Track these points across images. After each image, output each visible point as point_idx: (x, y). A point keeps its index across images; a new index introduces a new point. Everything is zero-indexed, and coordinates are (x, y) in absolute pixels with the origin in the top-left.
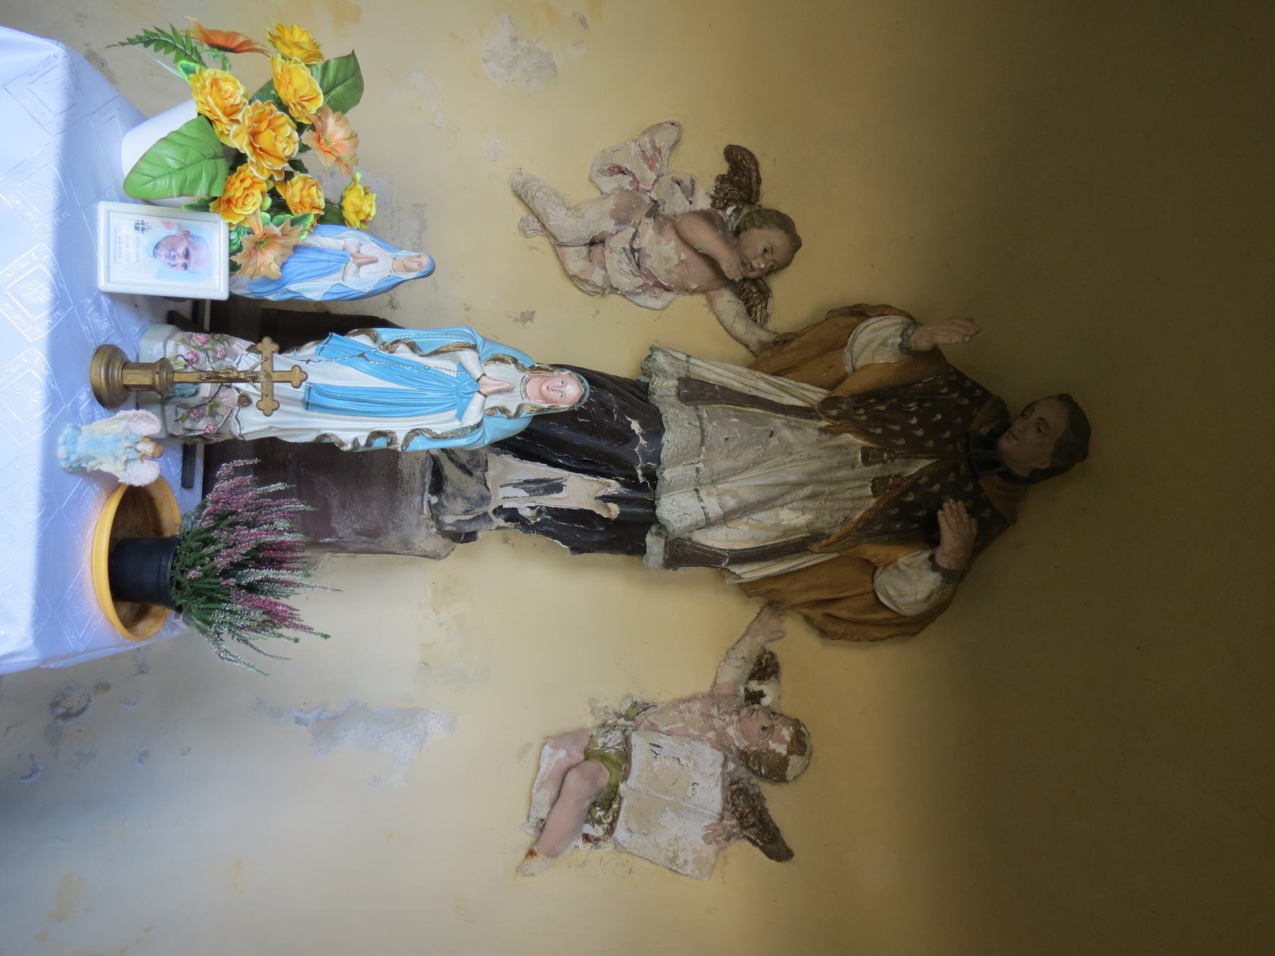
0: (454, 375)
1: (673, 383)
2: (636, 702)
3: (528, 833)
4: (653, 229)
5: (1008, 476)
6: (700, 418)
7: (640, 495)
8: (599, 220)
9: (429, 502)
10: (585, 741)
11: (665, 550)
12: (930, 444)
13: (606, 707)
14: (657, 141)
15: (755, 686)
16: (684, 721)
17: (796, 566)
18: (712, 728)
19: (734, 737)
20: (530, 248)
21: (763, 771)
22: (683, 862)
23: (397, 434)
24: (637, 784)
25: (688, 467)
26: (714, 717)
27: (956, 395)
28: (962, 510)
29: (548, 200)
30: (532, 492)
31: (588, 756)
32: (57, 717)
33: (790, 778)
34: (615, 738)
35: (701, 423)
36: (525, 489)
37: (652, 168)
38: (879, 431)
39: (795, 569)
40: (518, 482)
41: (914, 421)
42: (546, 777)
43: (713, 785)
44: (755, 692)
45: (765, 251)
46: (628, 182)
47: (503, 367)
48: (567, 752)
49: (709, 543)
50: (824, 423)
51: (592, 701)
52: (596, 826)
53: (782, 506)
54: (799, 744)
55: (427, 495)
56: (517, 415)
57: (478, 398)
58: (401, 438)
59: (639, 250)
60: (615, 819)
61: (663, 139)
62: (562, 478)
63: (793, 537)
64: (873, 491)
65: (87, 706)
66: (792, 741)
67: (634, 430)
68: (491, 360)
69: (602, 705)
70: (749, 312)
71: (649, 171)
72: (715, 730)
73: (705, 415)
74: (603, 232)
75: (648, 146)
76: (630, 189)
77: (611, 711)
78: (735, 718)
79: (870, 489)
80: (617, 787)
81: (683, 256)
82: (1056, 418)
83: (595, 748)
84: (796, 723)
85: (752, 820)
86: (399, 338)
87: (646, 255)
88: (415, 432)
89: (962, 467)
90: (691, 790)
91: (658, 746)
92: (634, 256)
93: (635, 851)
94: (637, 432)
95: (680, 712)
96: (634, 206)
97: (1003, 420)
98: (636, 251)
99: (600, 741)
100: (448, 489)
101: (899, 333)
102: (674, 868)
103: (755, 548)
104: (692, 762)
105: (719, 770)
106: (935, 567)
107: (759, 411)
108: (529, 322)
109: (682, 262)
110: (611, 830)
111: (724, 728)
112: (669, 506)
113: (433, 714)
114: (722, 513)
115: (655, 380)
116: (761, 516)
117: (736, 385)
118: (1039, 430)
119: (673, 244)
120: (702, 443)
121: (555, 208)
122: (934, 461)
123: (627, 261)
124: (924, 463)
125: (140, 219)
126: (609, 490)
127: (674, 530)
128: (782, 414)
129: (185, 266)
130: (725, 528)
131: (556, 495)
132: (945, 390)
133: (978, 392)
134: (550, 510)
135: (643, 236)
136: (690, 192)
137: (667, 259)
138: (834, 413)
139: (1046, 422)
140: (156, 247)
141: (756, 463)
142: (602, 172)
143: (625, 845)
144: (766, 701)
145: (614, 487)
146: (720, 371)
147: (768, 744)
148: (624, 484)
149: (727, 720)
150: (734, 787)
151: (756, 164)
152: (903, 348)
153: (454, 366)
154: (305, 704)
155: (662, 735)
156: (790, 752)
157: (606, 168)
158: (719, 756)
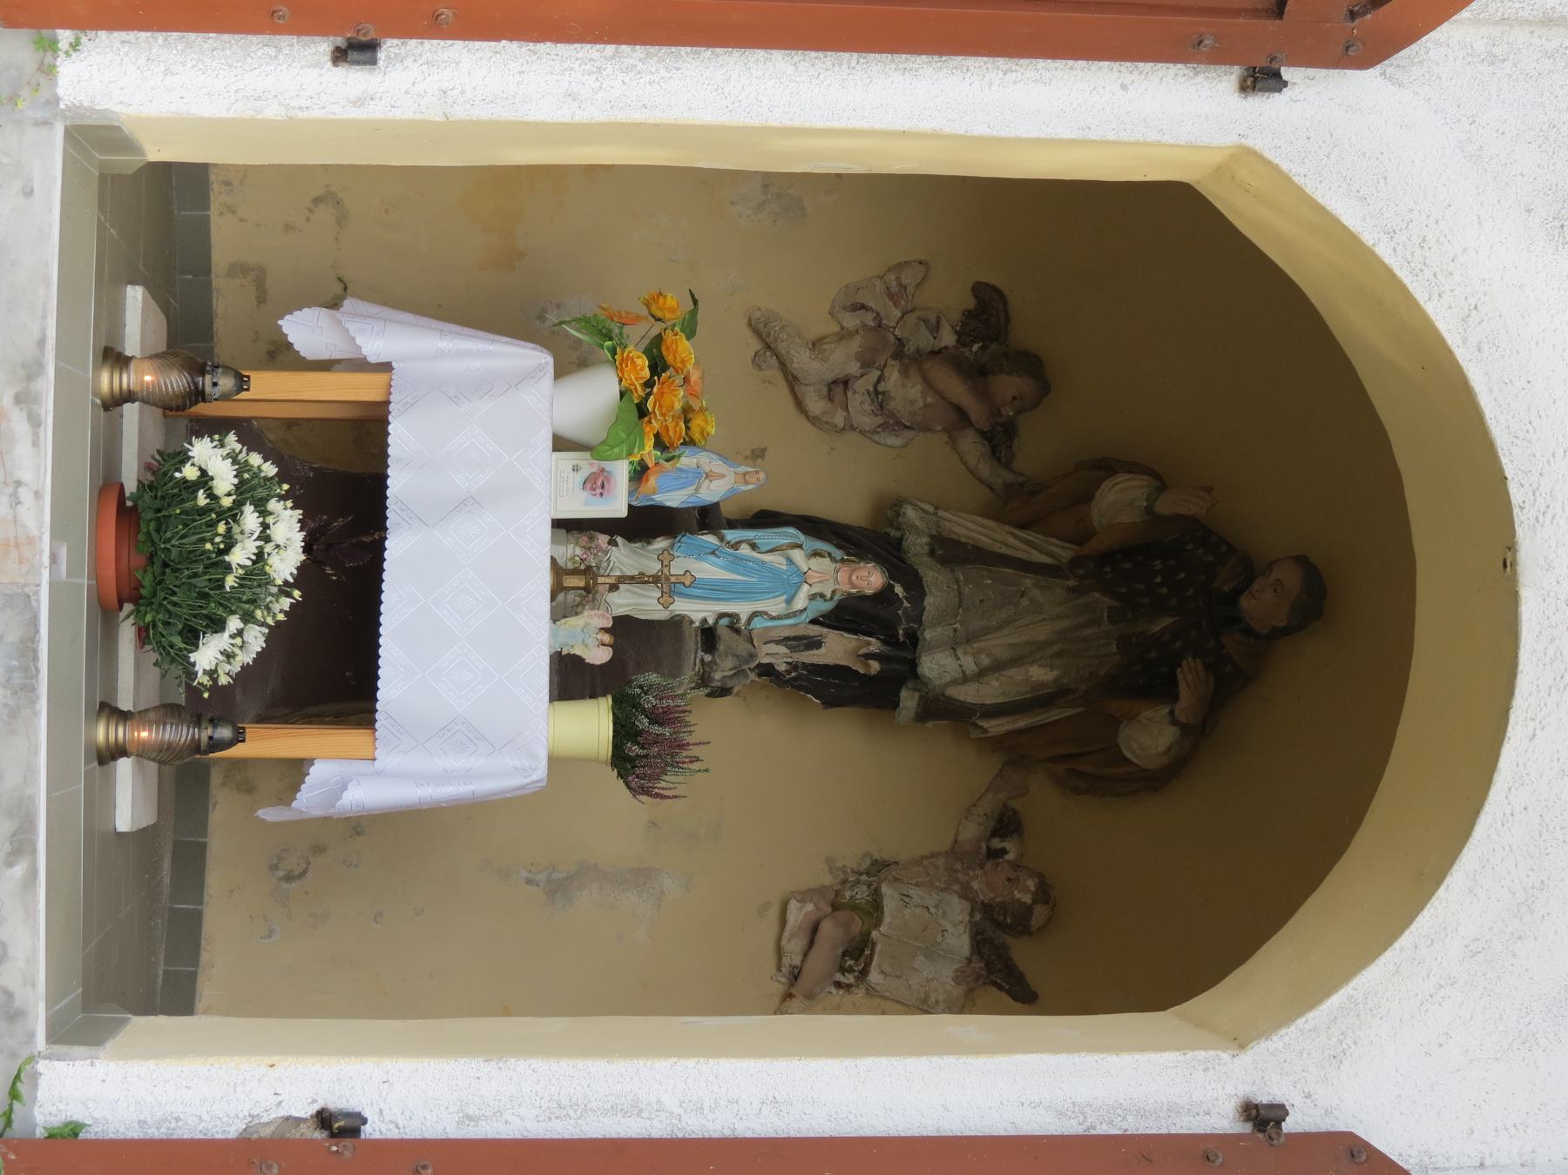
0: (785, 568)
1: (925, 540)
2: (876, 860)
3: (780, 982)
4: (899, 371)
5: (1248, 632)
6: (957, 581)
7: (900, 653)
8: (842, 359)
9: (702, 660)
10: (831, 896)
11: (919, 705)
12: (1174, 602)
13: (845, 866)
14: (903, 277)
15: (997, 843)
16: (929, 875)
17: (1043, 720)
18: (958, 881)
19: (979, 891)
20: (764, 382)
21: (1008, 920)
22: (934, 1002)
23: (741, 616)
24: (890, 931)
25: (946, 628)
26: (959, 872)
27: (1201, 551)
28: (1200, 667)
29: (792, 343)
30: (793, 649)
31: (835, 907)
32: (280, 879)
33: (1033, 929)
34: (862, 894)
35: (959, 586)
36: (786, 646)
37: (896, 304)
38: (1124, 590)
39: (1041, 723)
40: (777, 639)
41: (1158, 580)
42: (795, 929)
43: (962, 931)
44: (998, 850)
45: (1014, 398)
46: (871, 318)
47: (820, 560)
48: (815, 905)
49: (961, 698)
50: (1072, 583)
51: (830, 861)
52: (847, 974)
53: (1031, 664)
54: (1044, 893)
55: (700, 654)
56: (831, 599)
57: (806, 587)
58: (744, 618)
59: (883, 393)
60: (868, 964)
61: (909, 278)
62: (822, 635)
63: (1040, 693)
64: (1118, 648)
65: (307, 868)
66: (1037, 890)
67: (897, 594)
68: (812, 555)
69: (839, 864)
70: (994, 451)
71: (894, 309)
72: (961, 883)
73: (962, 578)
74: (848, 374)
75: (894, 283)
76: (873, 325)
77: (849, 870)
78: (979, 872)
79: (1115, 646)
80: (869, 934)
81: (929, 400)
82: (1290, 576)
83: (843, 901)
84: (1041, 877)
85: (998, 966)
86: (741, 539)
87: (891, 398)
88: (754, 615)
89: (1204, 624)
90: (940, 936)
91: (907, 896)
92: (878, 398)
93: (887, 994)
94: (901, 595)
95: (924, 868)
96: (880, 347)
97: (1249, 572)
98: (880, 393)
99: (848, 894)
100: (721, 647)
101: (1144, 497)
102: (925, 1008)
103: (1005, 703)
104: (941, 911)
105: (967, 918)
106: (1174, 721)
107: (1010, 571)
108: (760, 460)
109: (926, 406)
110: (864, 973)
111: (968, 883)
112: (929, 665)
113: (667, 874)
114: (978, 671)
115: (908, 537)
116: (1011, 672)
117: (985, 541)
118: (1275, 590)
119: (919, 387)
120: (960, 605)
121: (799, 350)
122: (1177, 618)
123: (870, 401)
124: (1166, 621)
125: (576, 462)
126: (871, 648)
127: (935, 687)
128: (1032, 573)
129: (601, 494)
130: (977, 683)
131: (815, 652)
132: (1190, 547)
133: (1224, 548)
134: (805, 666)
135: (889, 379)
136: (935, 329)
137: (912, 402)
138: (1081, 572)
139: (1282, 584)
140: (584, 483)
141: (1008, 622)
142: (845, 308)
143: (878, 988)
144: (1010, 856)
145: (875, 645)
146: (969, 525)
147: (1013, 893)
148: (885, 642)
149: (971, 875)
150: (979, 937)
151: (1005, 303)
152: (1149, 510)
153: (783, 561)
154: (532, 864)
155: (910, 886)
156: (1035, 902)
157: (849, 304)
158: (966, 906)
